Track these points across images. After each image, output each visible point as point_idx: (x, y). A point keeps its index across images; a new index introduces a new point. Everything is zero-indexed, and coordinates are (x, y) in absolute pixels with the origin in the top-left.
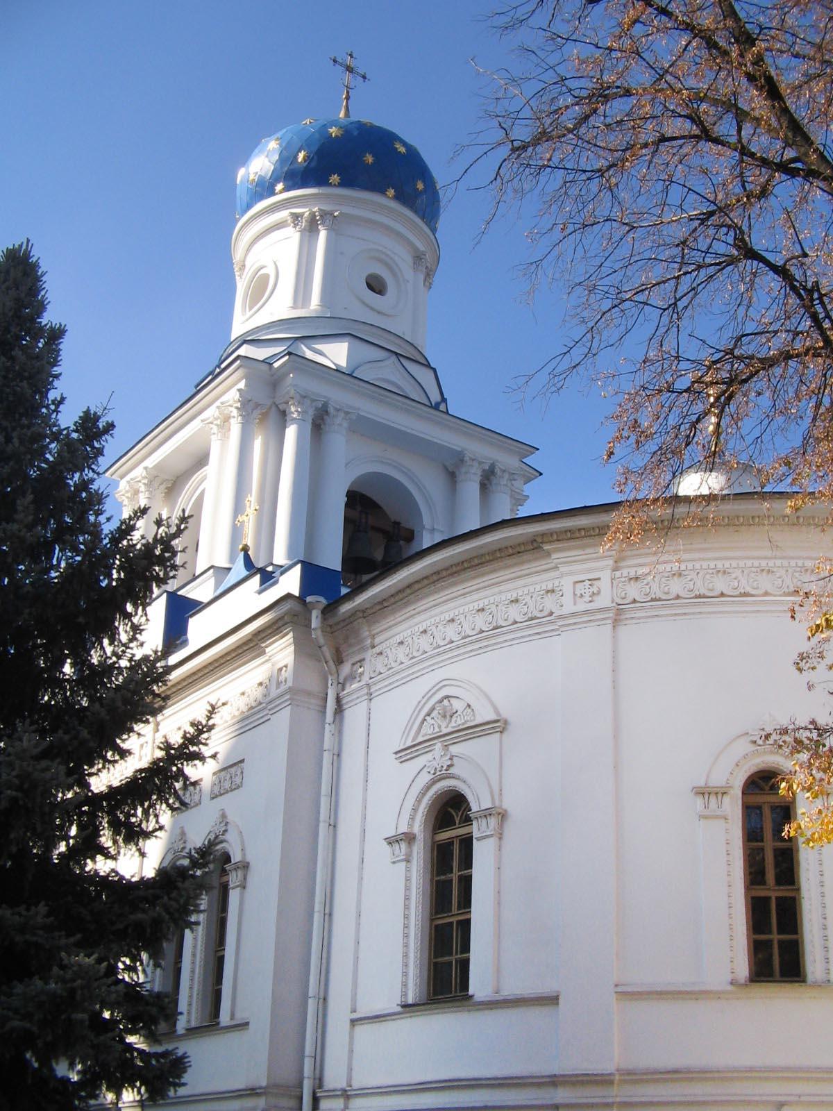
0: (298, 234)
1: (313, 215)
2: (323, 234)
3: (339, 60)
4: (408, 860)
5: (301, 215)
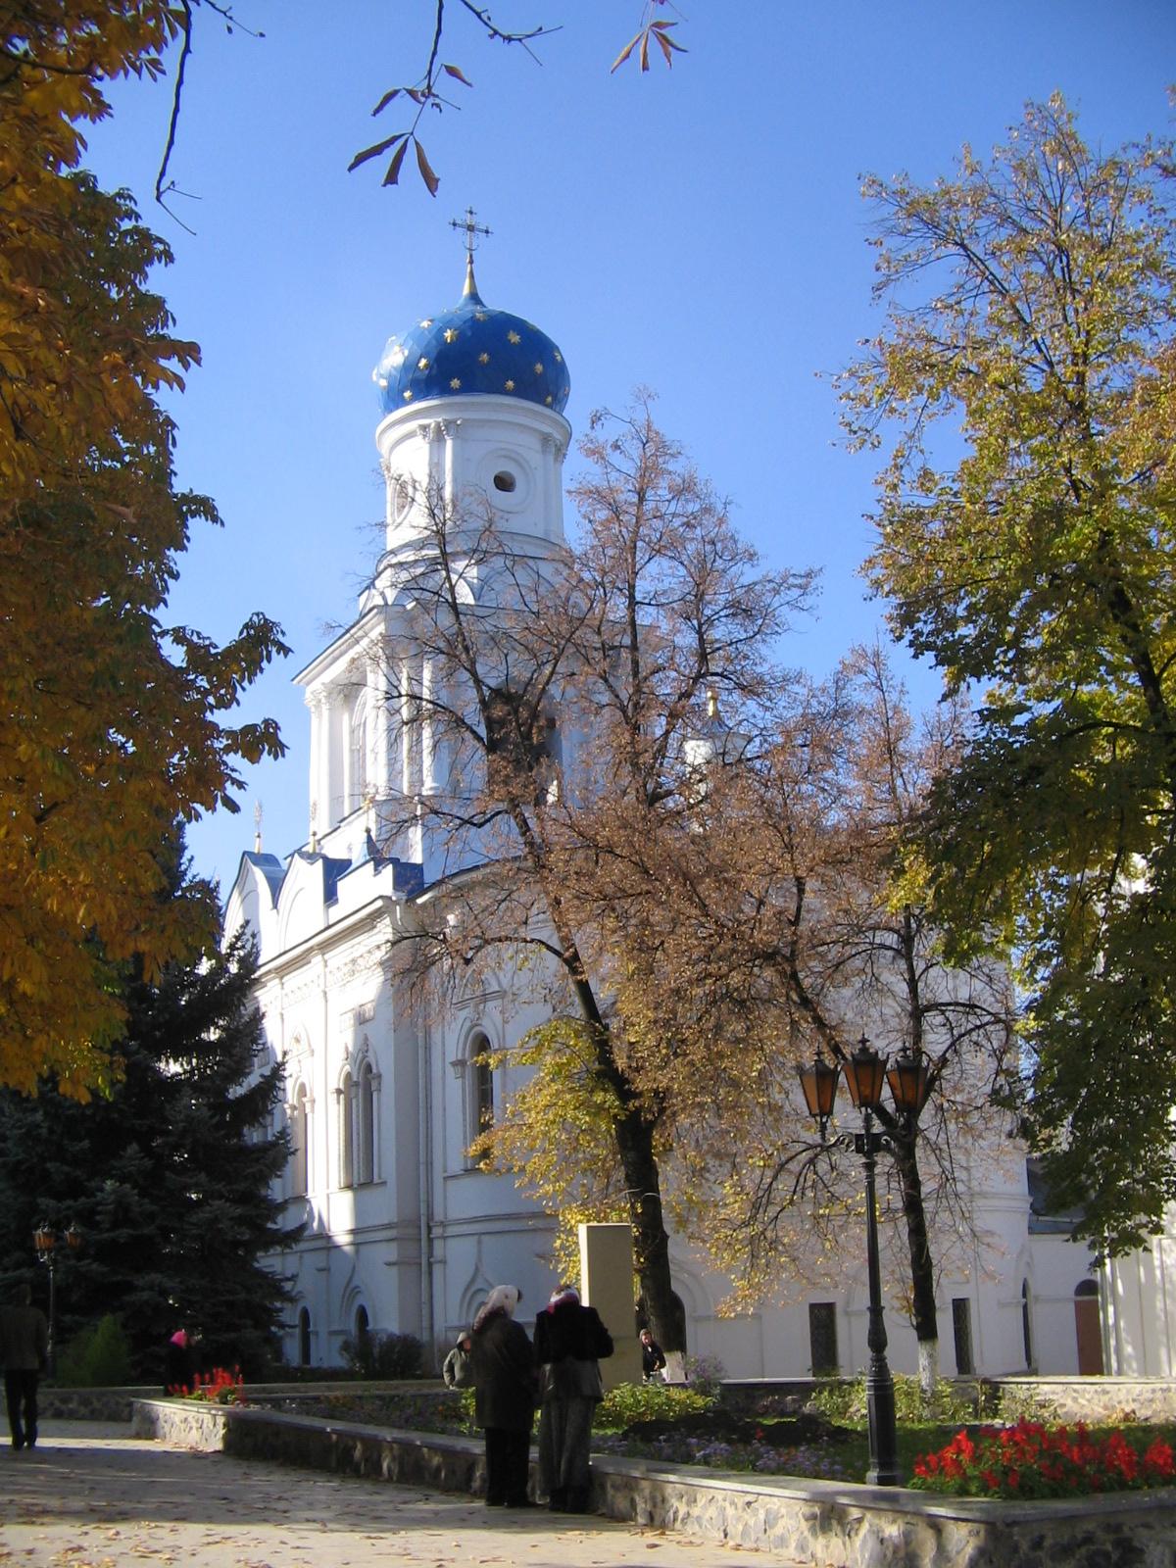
0: (427, 447)
1: (438, 425)
2: (449, 444)
3: (459, 222)
4: (463, 1077)
5: (429, 426)
